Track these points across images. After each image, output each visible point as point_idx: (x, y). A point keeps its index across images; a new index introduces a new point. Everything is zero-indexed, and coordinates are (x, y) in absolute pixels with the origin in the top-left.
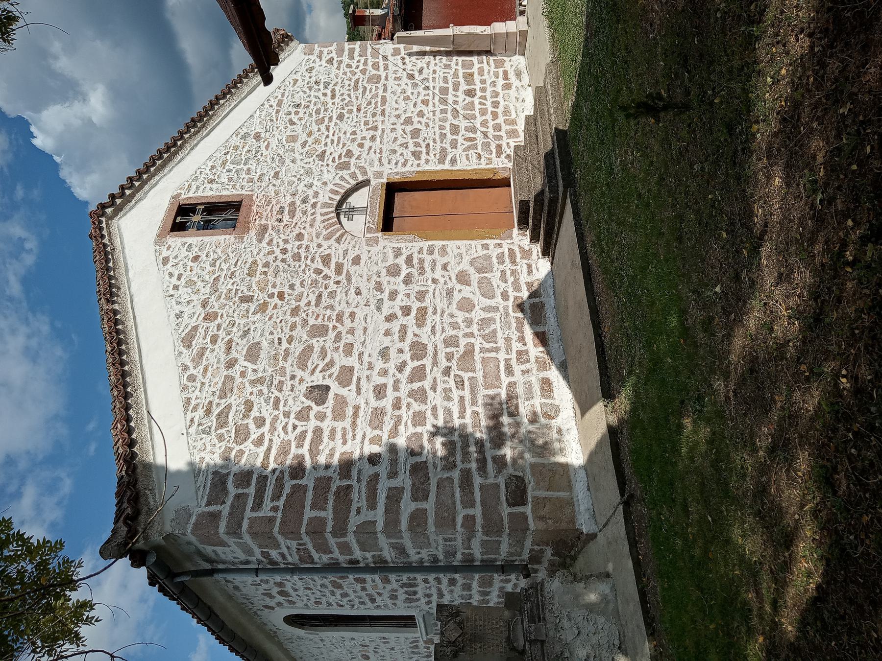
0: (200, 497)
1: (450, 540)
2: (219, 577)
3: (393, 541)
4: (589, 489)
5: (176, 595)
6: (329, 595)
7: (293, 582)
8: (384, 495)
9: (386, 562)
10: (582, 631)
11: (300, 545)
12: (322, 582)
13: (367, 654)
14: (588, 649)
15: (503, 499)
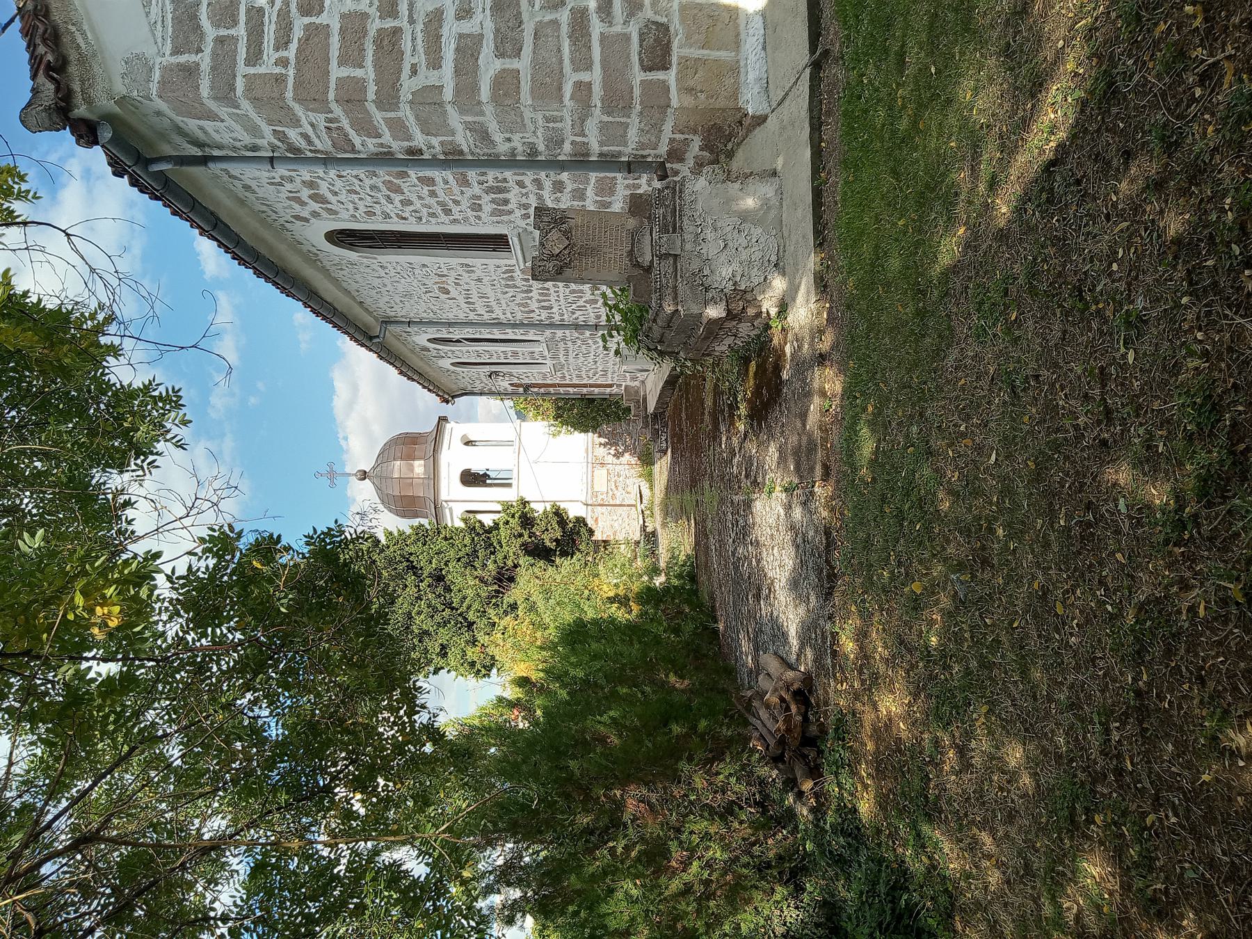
0: (159, 40)
1: (554, 120)
2: (215, 167)
3: (470, 119)
4: (764, 48)
5: (158, 191)
6: (383, 201)
7: (328, 179)
8: (453, 46)
9: (461, 152)
10: (730, 244)
11: (330, 121)
12: (372, 182)
13: (446, 286)
14: (735, 266)
15: (635, 58)
